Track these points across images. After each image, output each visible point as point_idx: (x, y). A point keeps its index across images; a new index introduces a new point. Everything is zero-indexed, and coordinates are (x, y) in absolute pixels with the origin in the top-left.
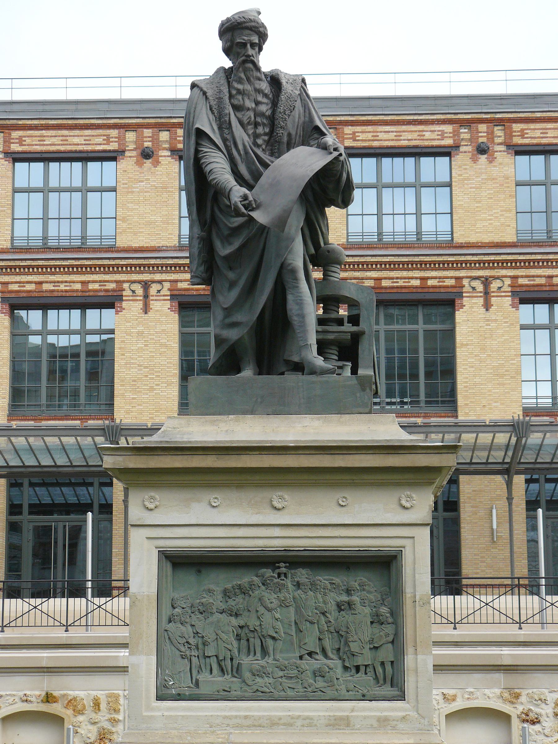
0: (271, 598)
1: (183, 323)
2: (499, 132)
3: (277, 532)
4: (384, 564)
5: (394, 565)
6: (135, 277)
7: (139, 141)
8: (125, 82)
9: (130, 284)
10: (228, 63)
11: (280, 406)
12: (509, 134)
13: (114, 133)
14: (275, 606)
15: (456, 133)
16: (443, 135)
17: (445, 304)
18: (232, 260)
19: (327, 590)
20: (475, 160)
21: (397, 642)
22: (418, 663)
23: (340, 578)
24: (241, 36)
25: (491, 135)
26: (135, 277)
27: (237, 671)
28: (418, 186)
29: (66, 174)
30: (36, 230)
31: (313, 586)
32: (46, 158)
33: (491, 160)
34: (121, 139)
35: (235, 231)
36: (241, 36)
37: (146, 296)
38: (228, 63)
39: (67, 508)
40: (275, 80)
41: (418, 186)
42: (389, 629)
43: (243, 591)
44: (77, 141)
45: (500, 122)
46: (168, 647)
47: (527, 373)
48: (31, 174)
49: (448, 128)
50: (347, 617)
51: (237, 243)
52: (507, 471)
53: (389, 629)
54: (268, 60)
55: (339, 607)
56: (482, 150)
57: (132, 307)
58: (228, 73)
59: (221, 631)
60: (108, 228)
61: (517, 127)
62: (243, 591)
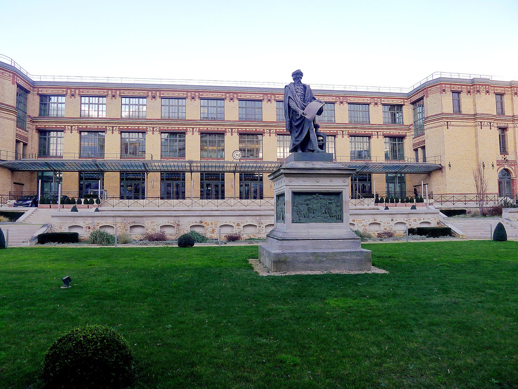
0: (316, 202)
1: (201, 137)
2: (273, 97)
3: (317, 187)
4: (338, 194)
5: (341, 195)
6: (190, 126)
7: (191, 94)
8: (109, 79)
9: (150, 128)
10: (293, 82)
11: (312, 159)
12: (238, 96)
13: (185, 93)
14: (315, 203)
15: (263, 96)
16: (144, 93)
17: (183, 134)
18: (298, 126)
19: (325, 200)
20: (230, 101)
21: (341, 210)
22: (345, 216)
23: (329, 197)
24: (298, 75)
25: (271, 97)
26: (190, 126)
27: (308, 217)
28: (139, 105)
29: (213, 103)
30: (167, 115)
31: (324, 199)
32: (130, 97)
33: (378, 106)
34: (187, 94)
35: (298, 120)
36: (298, 75)
37: (113, 130)
38: (293, 82)
39: (95, 179)
40: (305, 87)
41: (89, 104)
42: (340, 208)
43: (309, 200)
44: (176, 94)
45: (235, 93)
46: (294, 212)
47: (278, 151)
48: (165, 102)
49: (262, 95)
50: (330, 206)
51: (298, 123)
52: (234, 172)
53: (340, 208)
54: (304, 81)
55: (329, 203)
56: (269, 100)
57: (109, 133)
58: (294, 84)
59: (304, 208)
60: (184, 115)
61: (277, 96)
62: (309, 200)
